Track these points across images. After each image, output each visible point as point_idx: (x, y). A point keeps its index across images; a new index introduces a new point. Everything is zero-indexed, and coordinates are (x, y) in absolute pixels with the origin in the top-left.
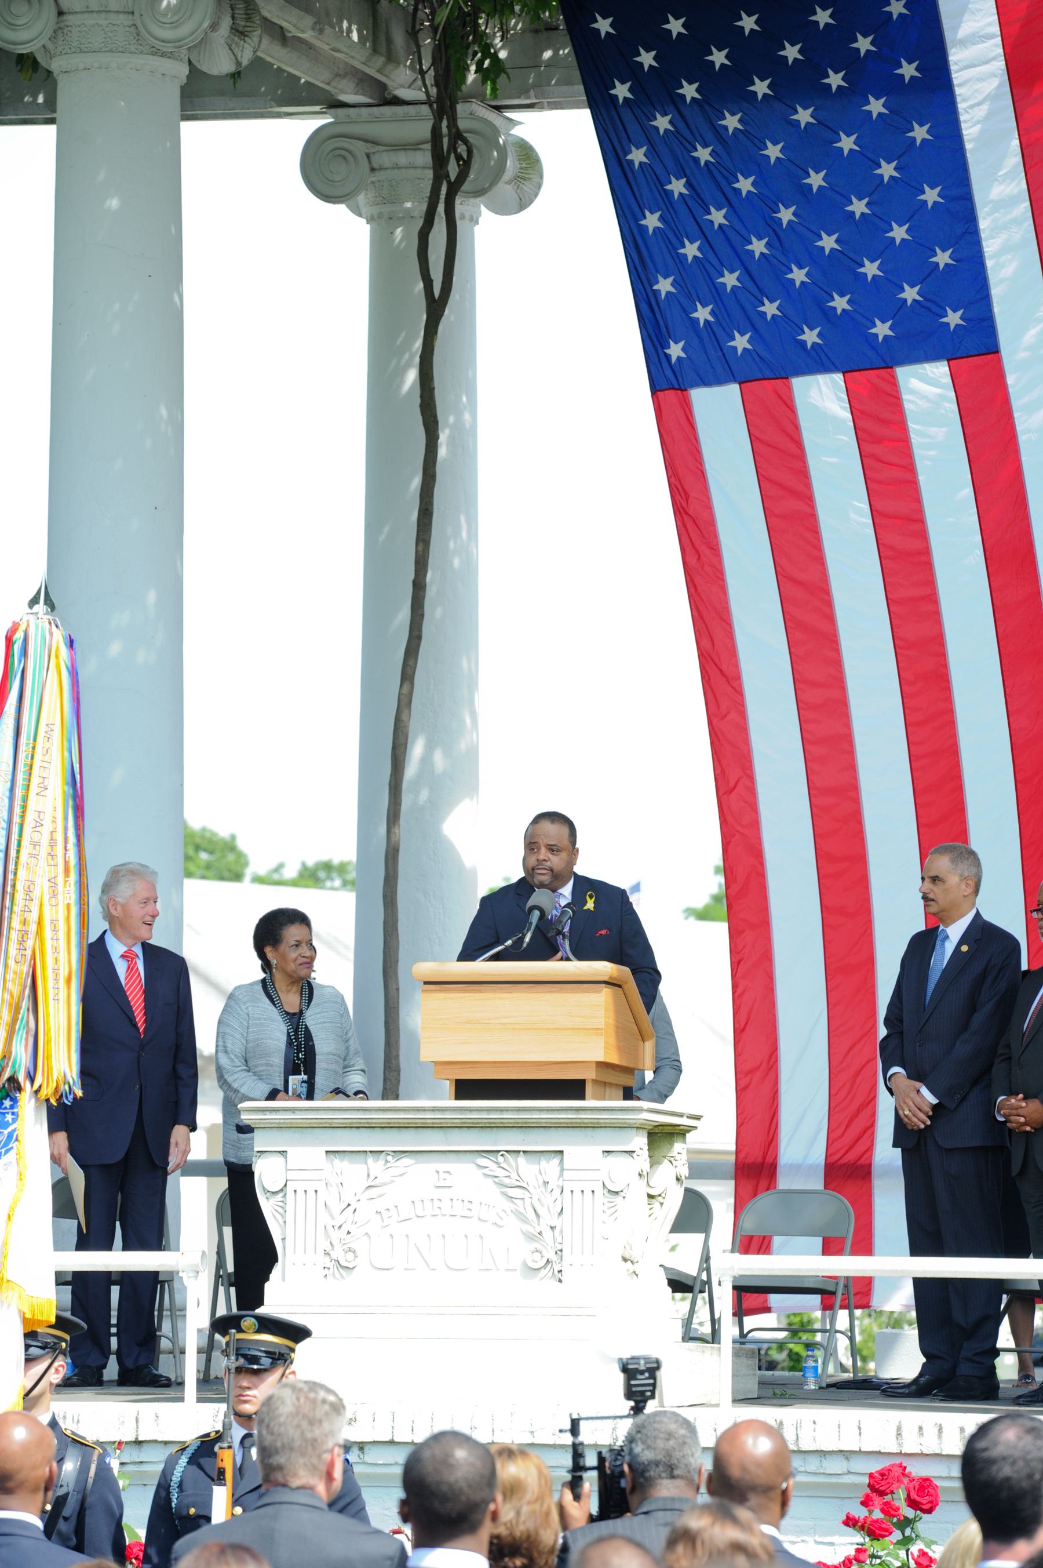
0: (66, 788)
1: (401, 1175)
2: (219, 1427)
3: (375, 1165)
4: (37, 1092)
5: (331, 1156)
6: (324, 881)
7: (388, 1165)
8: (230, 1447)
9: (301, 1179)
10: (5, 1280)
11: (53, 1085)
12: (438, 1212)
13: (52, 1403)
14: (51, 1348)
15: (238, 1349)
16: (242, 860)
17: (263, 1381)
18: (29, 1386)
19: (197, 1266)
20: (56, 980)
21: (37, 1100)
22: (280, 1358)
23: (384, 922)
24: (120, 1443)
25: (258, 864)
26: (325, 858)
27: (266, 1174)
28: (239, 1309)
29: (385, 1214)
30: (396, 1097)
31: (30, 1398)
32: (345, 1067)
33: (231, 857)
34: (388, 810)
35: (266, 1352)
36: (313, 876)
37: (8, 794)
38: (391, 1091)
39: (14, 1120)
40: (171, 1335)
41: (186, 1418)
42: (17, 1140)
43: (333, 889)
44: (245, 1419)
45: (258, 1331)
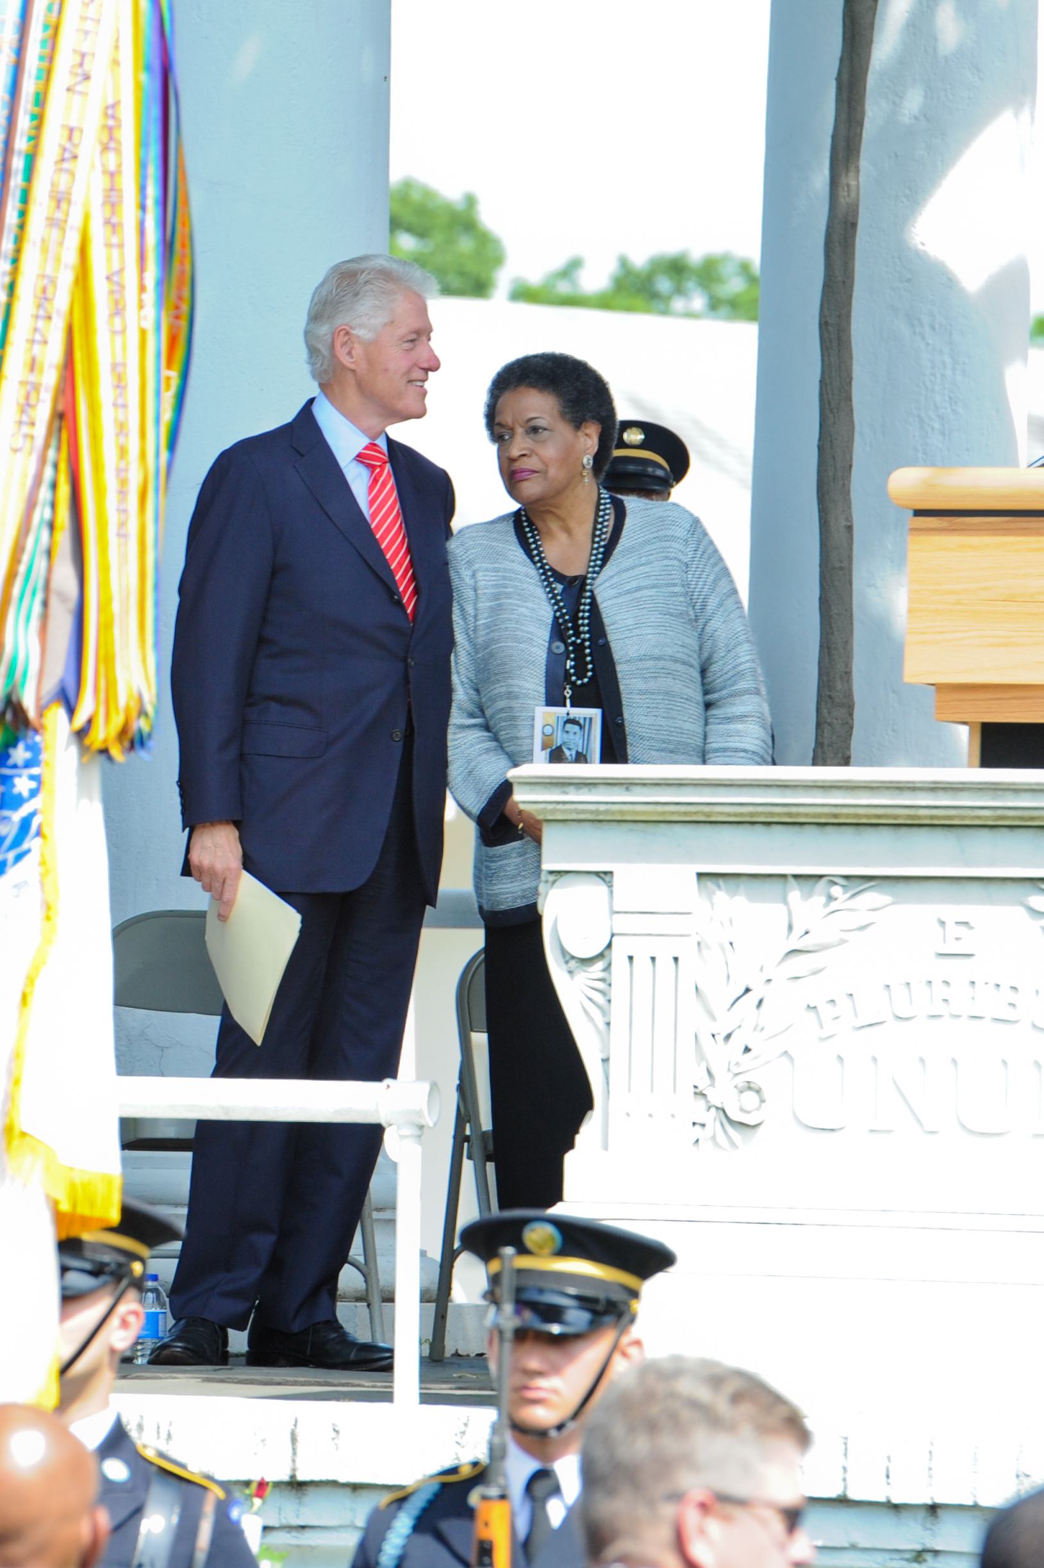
0: (144, 77)
1: (862, 928)
2: (481, 1454)
3: (806, 906)
4: (81, 734)
5: (710, 884)
6: (666, 299)
7: (834, 906)
8: (503, 1497)
9: (643, 933)
10: (16, 1131)
11: (117, 721)
12: (941, 1009)
13: (114, 1397)
14: (112, 1274)
15: (519, 1290)
16: (489, 252)
17: (571, 1358)
18: (68, 1352)
19: (419, 1113)
20: (122, 493)
21: (84, 749)
22: (608, 1311)
23: (822, 382)
24: (262, 1485)
25: (524, 261)
26: (670, 247)
27: (568, 920)
28: (502, 1206)
29: (825, 1010)
30: (846, 761)
31: (72, 1383)
32: (708, 706)
33: (466, 245)
34: (834, 137)
35: (578, 1298)
36: (643, 288)
37: (7, 97)
38: (832, 746)
39: (34, 793)
40: (361, 1259)
41: (404, 1436)
42: (39, 833)
43: (690, 315)
44: (535, 1438)
45: (564, 1251)
